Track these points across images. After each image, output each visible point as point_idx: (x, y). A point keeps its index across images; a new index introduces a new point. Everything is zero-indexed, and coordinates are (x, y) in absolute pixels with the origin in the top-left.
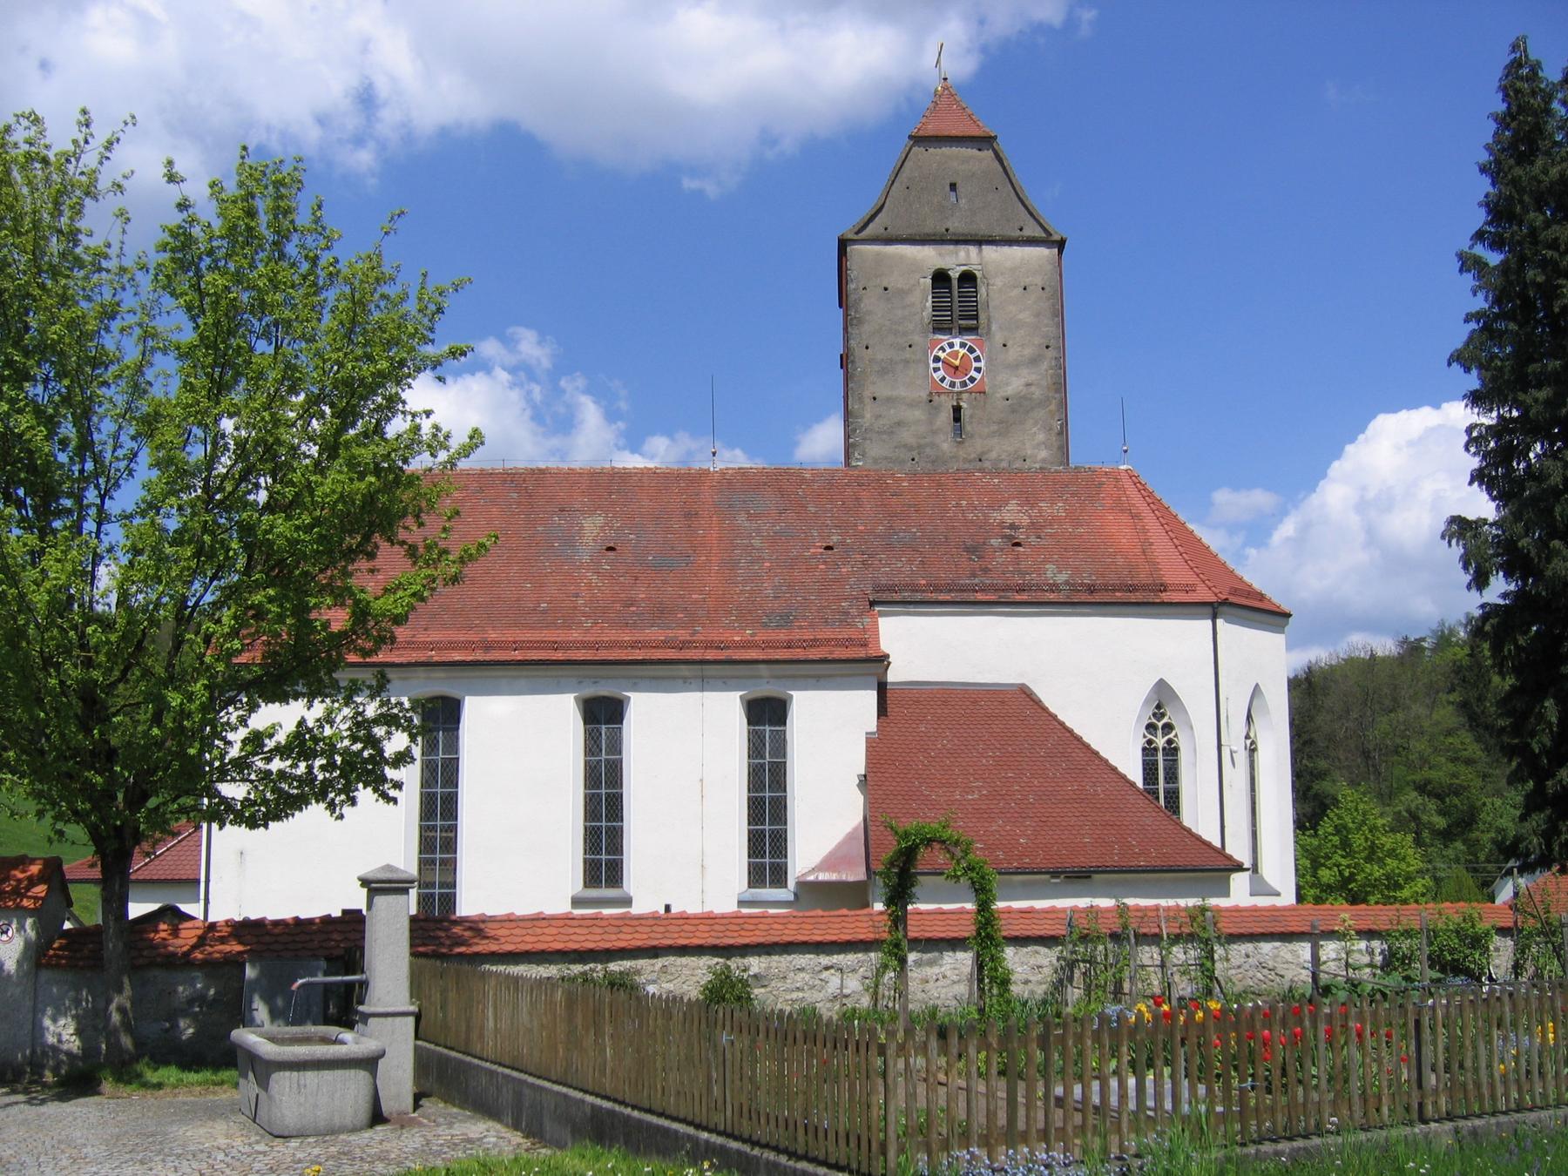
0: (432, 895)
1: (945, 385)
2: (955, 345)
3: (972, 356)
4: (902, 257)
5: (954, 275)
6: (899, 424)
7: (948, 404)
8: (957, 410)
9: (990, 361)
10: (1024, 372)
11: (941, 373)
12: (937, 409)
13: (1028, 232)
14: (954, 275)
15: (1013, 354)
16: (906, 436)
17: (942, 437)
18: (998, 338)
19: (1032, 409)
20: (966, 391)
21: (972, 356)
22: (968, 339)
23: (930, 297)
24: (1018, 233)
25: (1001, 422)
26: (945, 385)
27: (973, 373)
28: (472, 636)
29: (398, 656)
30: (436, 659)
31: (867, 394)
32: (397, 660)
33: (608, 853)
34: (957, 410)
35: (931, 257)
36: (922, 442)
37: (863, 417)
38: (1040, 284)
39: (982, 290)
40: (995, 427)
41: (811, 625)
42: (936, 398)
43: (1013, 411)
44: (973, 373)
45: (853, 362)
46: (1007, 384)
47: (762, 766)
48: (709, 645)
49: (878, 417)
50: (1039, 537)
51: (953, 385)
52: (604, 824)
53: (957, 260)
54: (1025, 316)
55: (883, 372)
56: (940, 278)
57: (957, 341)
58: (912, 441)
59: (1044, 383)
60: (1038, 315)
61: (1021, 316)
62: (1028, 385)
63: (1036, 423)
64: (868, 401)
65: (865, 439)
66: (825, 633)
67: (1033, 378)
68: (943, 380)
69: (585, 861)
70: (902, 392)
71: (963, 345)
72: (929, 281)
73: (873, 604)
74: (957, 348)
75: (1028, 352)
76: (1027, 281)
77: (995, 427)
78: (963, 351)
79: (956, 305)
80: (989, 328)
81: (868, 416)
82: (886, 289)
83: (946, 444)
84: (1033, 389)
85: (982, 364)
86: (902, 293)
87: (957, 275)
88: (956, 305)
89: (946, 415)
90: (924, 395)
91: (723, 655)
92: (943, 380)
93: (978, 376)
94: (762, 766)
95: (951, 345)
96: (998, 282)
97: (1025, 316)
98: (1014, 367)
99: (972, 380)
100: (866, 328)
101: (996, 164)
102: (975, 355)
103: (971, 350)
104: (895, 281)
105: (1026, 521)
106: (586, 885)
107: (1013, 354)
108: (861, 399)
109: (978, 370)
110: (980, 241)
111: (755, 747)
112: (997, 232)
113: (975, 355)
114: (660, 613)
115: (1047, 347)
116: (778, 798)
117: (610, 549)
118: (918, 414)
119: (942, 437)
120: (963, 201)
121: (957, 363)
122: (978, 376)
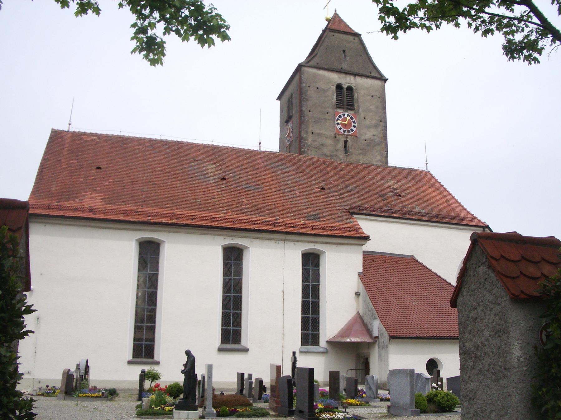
0: (141, 345)
1: (341, 131)
2: (347, 115)
3: (352, 121)
4: (324, 76)
5: (345, 86)
6: (323, 145)
7: (342, 139)
8: (346, 142)
9: (359, 124)
10: (372, 130)
11: (340, 126)
12: (338, 140)
13: (373, 74)
14: (345, 86)
15: (367, 122)
16: (326, 151)
17: (340, 153)
18: (362, 115)
19: (375, 145)
20: (349, 135)
21: (352, 121)
22: (351, 113)
23: (335, 94)
24: (370, 74)
25: (363, 149)
26: (341, 131)
27: (352, 128)
28: (167, 211)
29: (131, 218)
30: (153, 221)
31: (310, 130)
32: (131, 219)
33: (234, 326)
34: (346, 142)
35: (336, 78)
36: (332, 154)
37: (307, 140)
38: (378, 96)
39: (356, 95)
40: (361, 151)
41: (328, 221)
42: (337, 136)
43: (368, 146)
44: (352, 128)
45: (304, 116)
46: (366, 134)
47: (308, 286)
48: (287, 225)
49: (314, 141)
50: (406, 194)
51: (344, 131)
52: (232, 311)
53: (347, 81)
54: (373, 107)
55: (317, 122)
56: (339, 87)
57: (346, 114)
58: (328, 153)
59: (380, 136)
60: (377, 107)
61: (371, 107)
62: (374, 135)
63: (377, 152)
64: (310, 134)
65: (309, 150)
66: (337, 225)
67: (375, 133)
68: (340, 129)
69: (222, 329)
70: (324, 132)
71: (348, 115)
72: (335, 87)
73: (352, 214)
74: (346, 116)
75: (374, 122)
76: (373, 94)
77: (361, 151)
78: (348, 118)
79: (345, 99)
80: (358, 110)
81: (310, 140)
82: (317, 88)
83: (341, 155)
84: (375, 137)
85: (356, 125)
86: (324, 91)
87: (346, 87)
88: (345, 99)
89: (341, 144)
90: (332, 134)
91: (295, 230)
92: (340, 129)
93: (354, 129)
94: (308, 286)
95: (344, 115)
96: (362, 92)
97: (373, 107)
98: (369, 127)
99: (352, 130)
100: (309, 103)
101: (360, 46)
102: (353, 120)
103: (352, 118)
104: (321, 85)
105: (398, 187)
106: (133, 357)
107: (367, 122)
108: (307, 132)
109: (354, 127)
110: (355, 75)
111: (305, 277)
112: (361, 72)
113: (353, 120)
114: (257, 210)
115: (381, 121)
116: (315, 302)
117: (224, 179)
118: (329, 142)
119: (340, 153)
120: (348, 58)
121: (346, 123)
122: (354, 129)
